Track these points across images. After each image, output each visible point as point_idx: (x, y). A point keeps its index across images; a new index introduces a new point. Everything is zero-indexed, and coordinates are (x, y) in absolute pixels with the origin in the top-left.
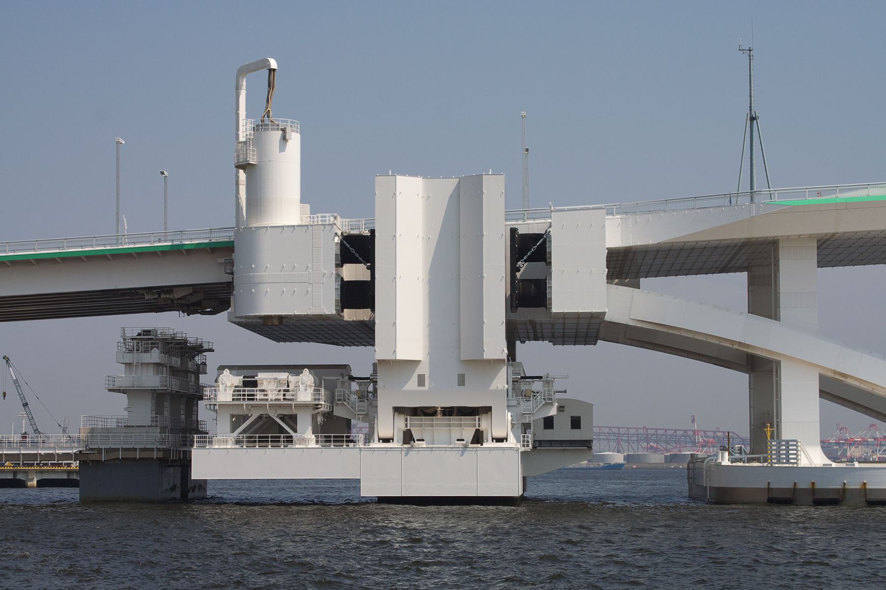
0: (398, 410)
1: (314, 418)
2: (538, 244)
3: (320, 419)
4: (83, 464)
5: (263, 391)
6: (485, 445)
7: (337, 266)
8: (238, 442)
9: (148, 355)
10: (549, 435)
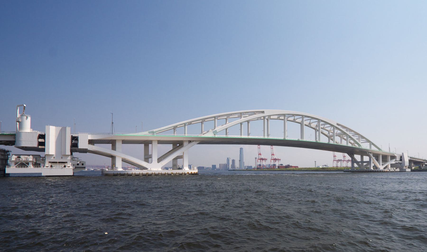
0: (50, 162)
1: (33, 163)
3: (34, 163)
6: (66, 168)
7: (38, 139)
10: (78, 166)
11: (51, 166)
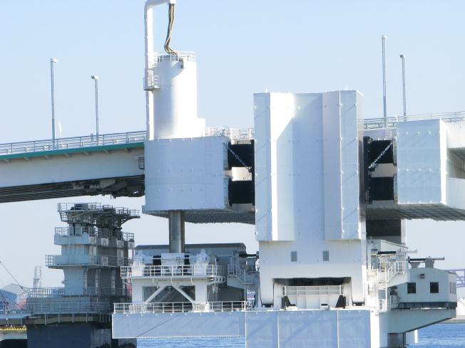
0: (278, 281)
1: (209, 288)
2: (386, 150)
3: (215, 289)
4: (30, 327)
5: (166, 268)
6: (347, 308)
10: (412, 298)
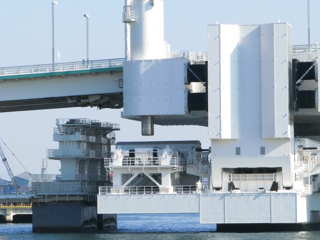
0: (225, 170)
1: (172, 175)
2: (310, 69)
3: (177, 176)
4: (35, 204)
6: (279, 191)
7: (186, 84)
8: (126, 191)
9: (73, 136)
11: (231, 186)
